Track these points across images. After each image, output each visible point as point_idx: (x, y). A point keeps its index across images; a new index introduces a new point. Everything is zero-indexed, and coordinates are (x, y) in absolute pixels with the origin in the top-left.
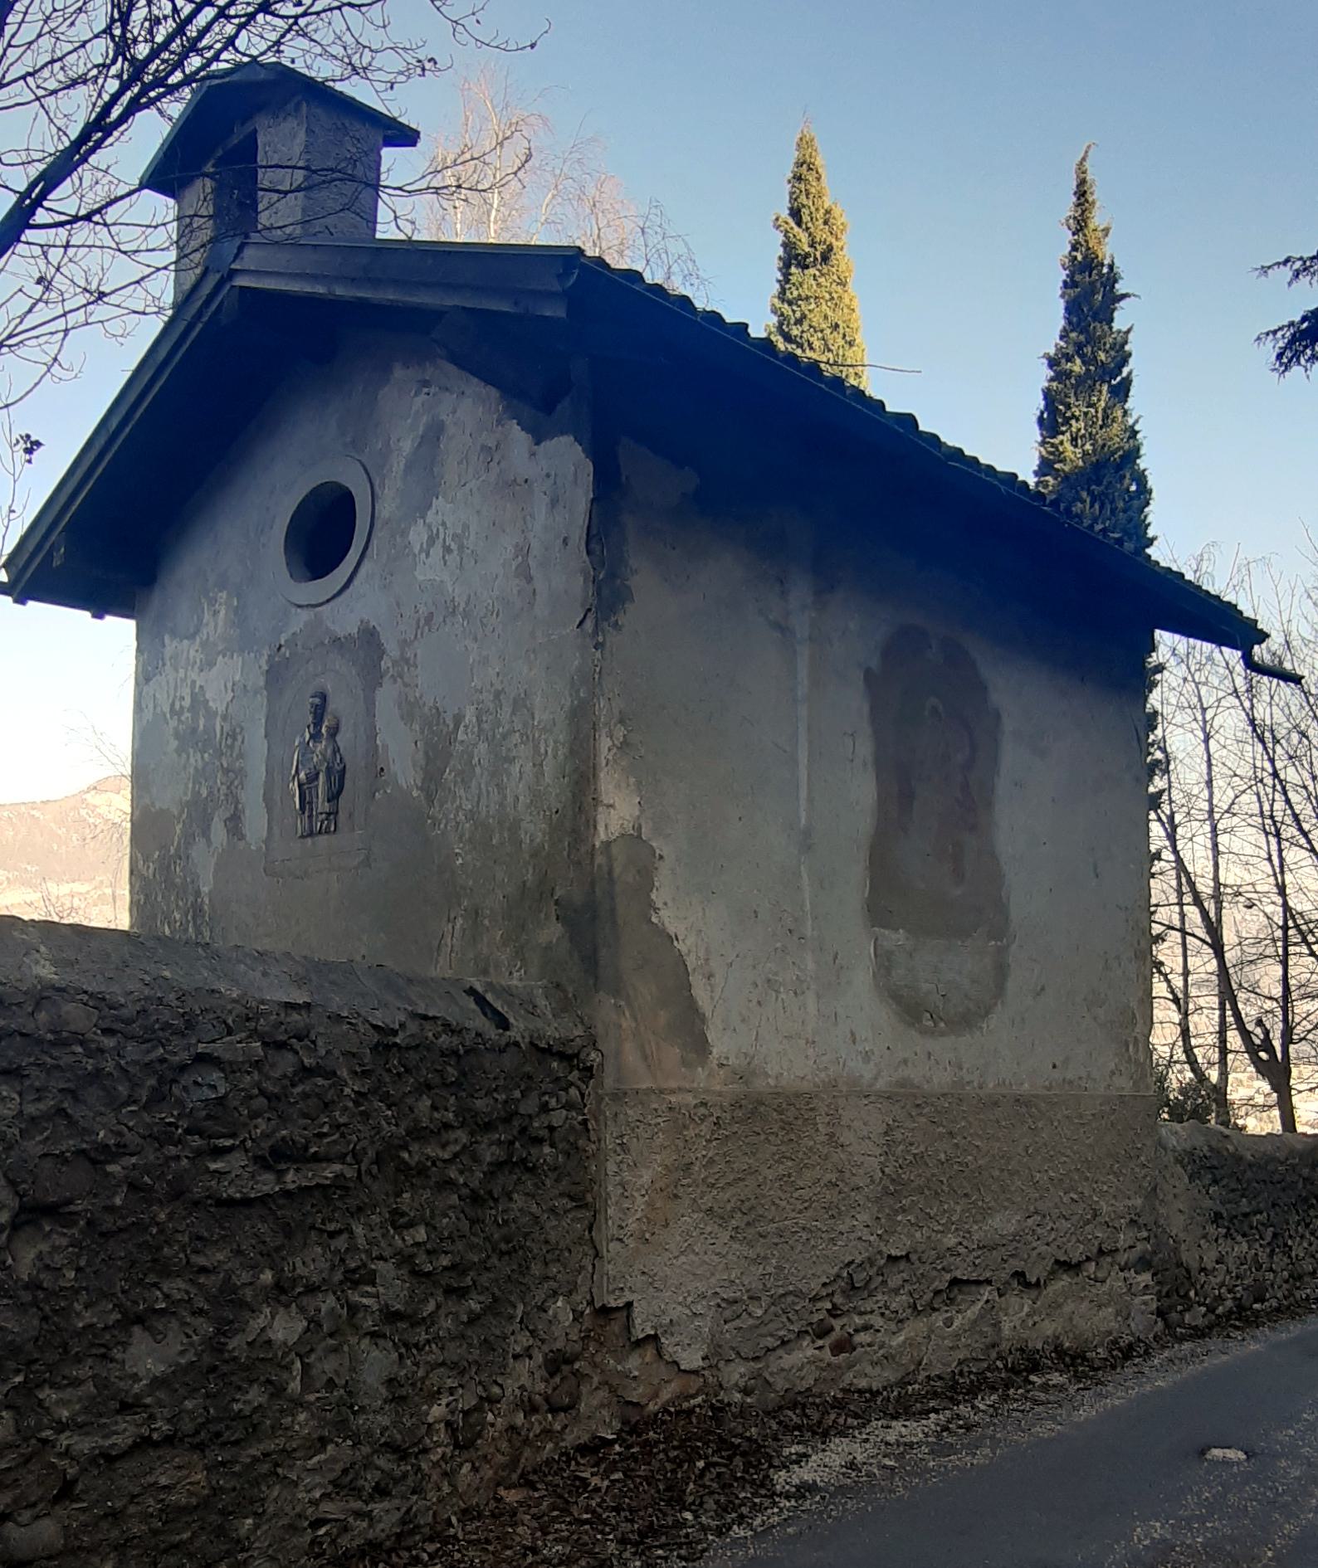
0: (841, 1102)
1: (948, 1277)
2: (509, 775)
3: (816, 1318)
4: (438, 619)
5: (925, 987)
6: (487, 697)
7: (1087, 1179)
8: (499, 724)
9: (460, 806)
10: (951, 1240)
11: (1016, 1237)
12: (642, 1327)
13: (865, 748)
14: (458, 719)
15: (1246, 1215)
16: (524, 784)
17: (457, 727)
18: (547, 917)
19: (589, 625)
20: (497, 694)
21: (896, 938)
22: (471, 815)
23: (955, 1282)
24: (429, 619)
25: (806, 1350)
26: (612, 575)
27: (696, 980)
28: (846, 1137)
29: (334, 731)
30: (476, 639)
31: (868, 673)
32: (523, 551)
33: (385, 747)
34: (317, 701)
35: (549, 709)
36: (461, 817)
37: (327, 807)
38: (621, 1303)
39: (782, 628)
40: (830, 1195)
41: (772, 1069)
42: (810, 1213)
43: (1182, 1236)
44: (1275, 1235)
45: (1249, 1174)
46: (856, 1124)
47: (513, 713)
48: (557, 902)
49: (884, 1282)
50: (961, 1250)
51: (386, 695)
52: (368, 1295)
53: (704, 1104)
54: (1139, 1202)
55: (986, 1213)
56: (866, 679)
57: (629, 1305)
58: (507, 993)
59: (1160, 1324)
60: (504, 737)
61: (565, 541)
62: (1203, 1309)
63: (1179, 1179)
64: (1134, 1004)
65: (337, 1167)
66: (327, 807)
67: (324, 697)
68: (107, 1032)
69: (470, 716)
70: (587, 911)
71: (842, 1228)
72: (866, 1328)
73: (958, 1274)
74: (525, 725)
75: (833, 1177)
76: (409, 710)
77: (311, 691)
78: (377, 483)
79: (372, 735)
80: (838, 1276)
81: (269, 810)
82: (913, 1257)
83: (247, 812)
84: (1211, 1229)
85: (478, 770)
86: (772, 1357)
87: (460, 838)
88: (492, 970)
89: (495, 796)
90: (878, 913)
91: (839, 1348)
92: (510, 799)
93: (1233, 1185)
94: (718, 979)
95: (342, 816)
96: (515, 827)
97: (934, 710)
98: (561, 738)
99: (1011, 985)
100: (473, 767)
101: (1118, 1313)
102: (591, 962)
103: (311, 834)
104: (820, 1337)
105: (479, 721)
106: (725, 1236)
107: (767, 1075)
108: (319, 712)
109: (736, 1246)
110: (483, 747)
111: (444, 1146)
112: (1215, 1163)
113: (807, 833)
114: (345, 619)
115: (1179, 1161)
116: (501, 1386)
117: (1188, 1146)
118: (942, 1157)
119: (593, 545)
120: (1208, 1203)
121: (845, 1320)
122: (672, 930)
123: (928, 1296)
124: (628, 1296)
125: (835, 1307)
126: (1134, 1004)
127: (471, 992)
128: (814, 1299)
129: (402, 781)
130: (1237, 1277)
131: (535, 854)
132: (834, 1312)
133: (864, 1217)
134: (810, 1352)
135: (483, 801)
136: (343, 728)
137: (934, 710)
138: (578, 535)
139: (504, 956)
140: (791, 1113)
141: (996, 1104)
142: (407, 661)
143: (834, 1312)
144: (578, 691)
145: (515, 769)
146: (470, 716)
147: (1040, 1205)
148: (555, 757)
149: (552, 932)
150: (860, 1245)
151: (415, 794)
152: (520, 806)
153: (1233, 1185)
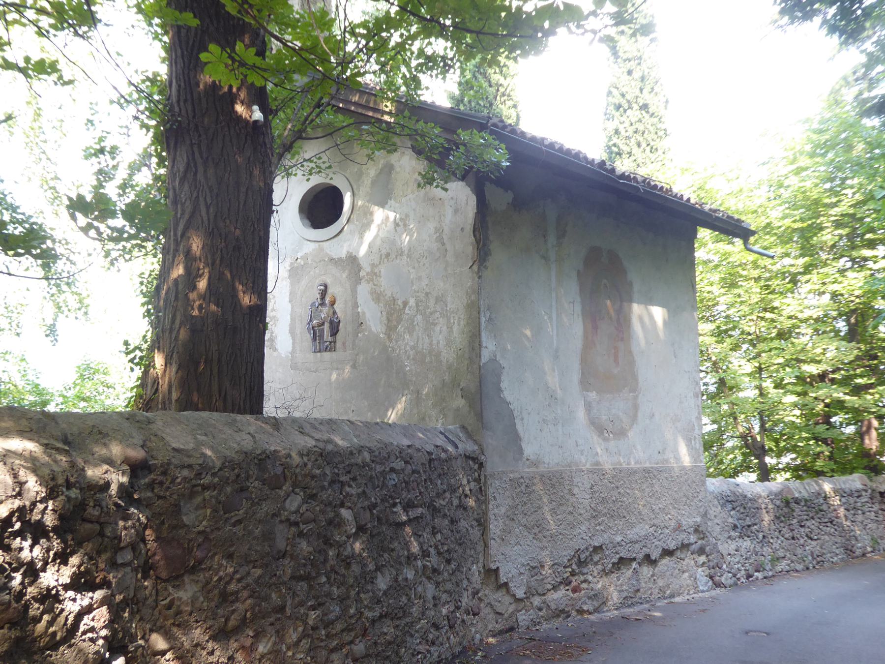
0: (574, 474)
1: (618, 556)
2: (434, 331)
3: (566, 575)
4: (393, 256)
5: (604, 418)
6: (422, 296)
7: (675, 508)
8: (427, 307)
9: (407, 344)
10: (619, 538)
11: (646, 537)
12: (503, 579)
13: (578, 308)
14: (405, 304)
15: (749, 526)
16: (445, 336)
17: (405, 307)
18: (457, 396)
19: (475, 268)
20: (427, 294)
21: (593, 395)
22: (413, 348)
23: (621, 559)
24: (388, 255)
25: (561, 592)
26: (484, 245)
27: (517, 421)
28: (576, 491)
29: (333, 303)
30: (414, 268)
31: (579, 272)
32: (439, 230)
33: (364, 313)
34: (322, 288)
35: (456, 302)
36: (408, 348)
37: (330, 339)
38: (494, 567)
39: (545, 258)
40: (570, 517)
41: (546, 460)
42: (562, 526)
43: (719, 537)
44: (764, 537)
45: (749, 505)
46: (580, 484)
47: (436, 303)
48: (462, 389)
49: (592, 559)
50: (624, 544)
51: (363, 290)
52: (427, 561)
53: (522, 477)
54: (699, 519)
55: (632, 526)
56: (578, 275)
57: (498, 568)
58: (450, 431)
59: (711, 583)
60: (431, 314)
61: (462, 229)
62: (730, 575)
63: (715, 510)
64: (694, 420)
65: (421, 509)
66: (330, 339)
67: (326, 286)
68: (373, 461)
69: (412, 302)
70: (477, 391)
71: (575, 533)
72: (585, 581)
73: (622, 555)
74: (442, 309)
75: (571, 509)
76: (377, 297)
77: (316, 284)
78: (355, 187)
79: (356, 305)
80: (574, 556)
81: (293, 338)
82: (604, 547)
83: (279, 338)
84: (733, 533)
85: (417, 328)
86: (549, 594)
87: (408, 358)
88: (427, 419)
89: (427, 340)
90: (585, 384)
91: (575, 590)
92: (435, 342)
93: (742, 510)
94: (525, 421)
95: (339, 344)
96: (439, 354)
97: (605, 284)
98: (462, 317)
99: (640, 414)
100: (414, 326)
101: (690, 577)
102: (480, 416)
103: (320, 351)
104: (567, 585)
105: (417, 305)
106: (531, 537)
107: (544, 463)
108: (323, 294)
109: (535, 541)
110: (419, 317)
111: (444, 499)
112: (733, 499)
113: (557, 351)
114: (339, 249)
115: (717, 498)
116: (297, 643)
117: (720, 491)
118: (614, 498)
119: (477, 233)
120: (730, 520)
121: (577, 577)
122: (508, 399)
123: (610, 566)
124: (498, 564)
125: (573, 570)
126: (694, 420)
127: (441, 433)
128: (565, 567)
129: (373, 329)
130: (746, 559)
131: (449, 367)
132: (573, 574)
133: (583, 528)
134: (564, 592)
135: (420, 342)
136: (337, 302)
137: (605, 284)
138: (469, 228)
139: (434, 413)
140: (555, 480)
141: (635, 472)
142: (375, 274)
143: (573, 574)
144: (470, 297)
145: (438, 328)
146: (412, 302)
147: (655, 521)
148: (459, 325)
149: (460, 402)
150: (582, 541)
151: (381, 336)
152: (440, 345)
153: (742, 510)
